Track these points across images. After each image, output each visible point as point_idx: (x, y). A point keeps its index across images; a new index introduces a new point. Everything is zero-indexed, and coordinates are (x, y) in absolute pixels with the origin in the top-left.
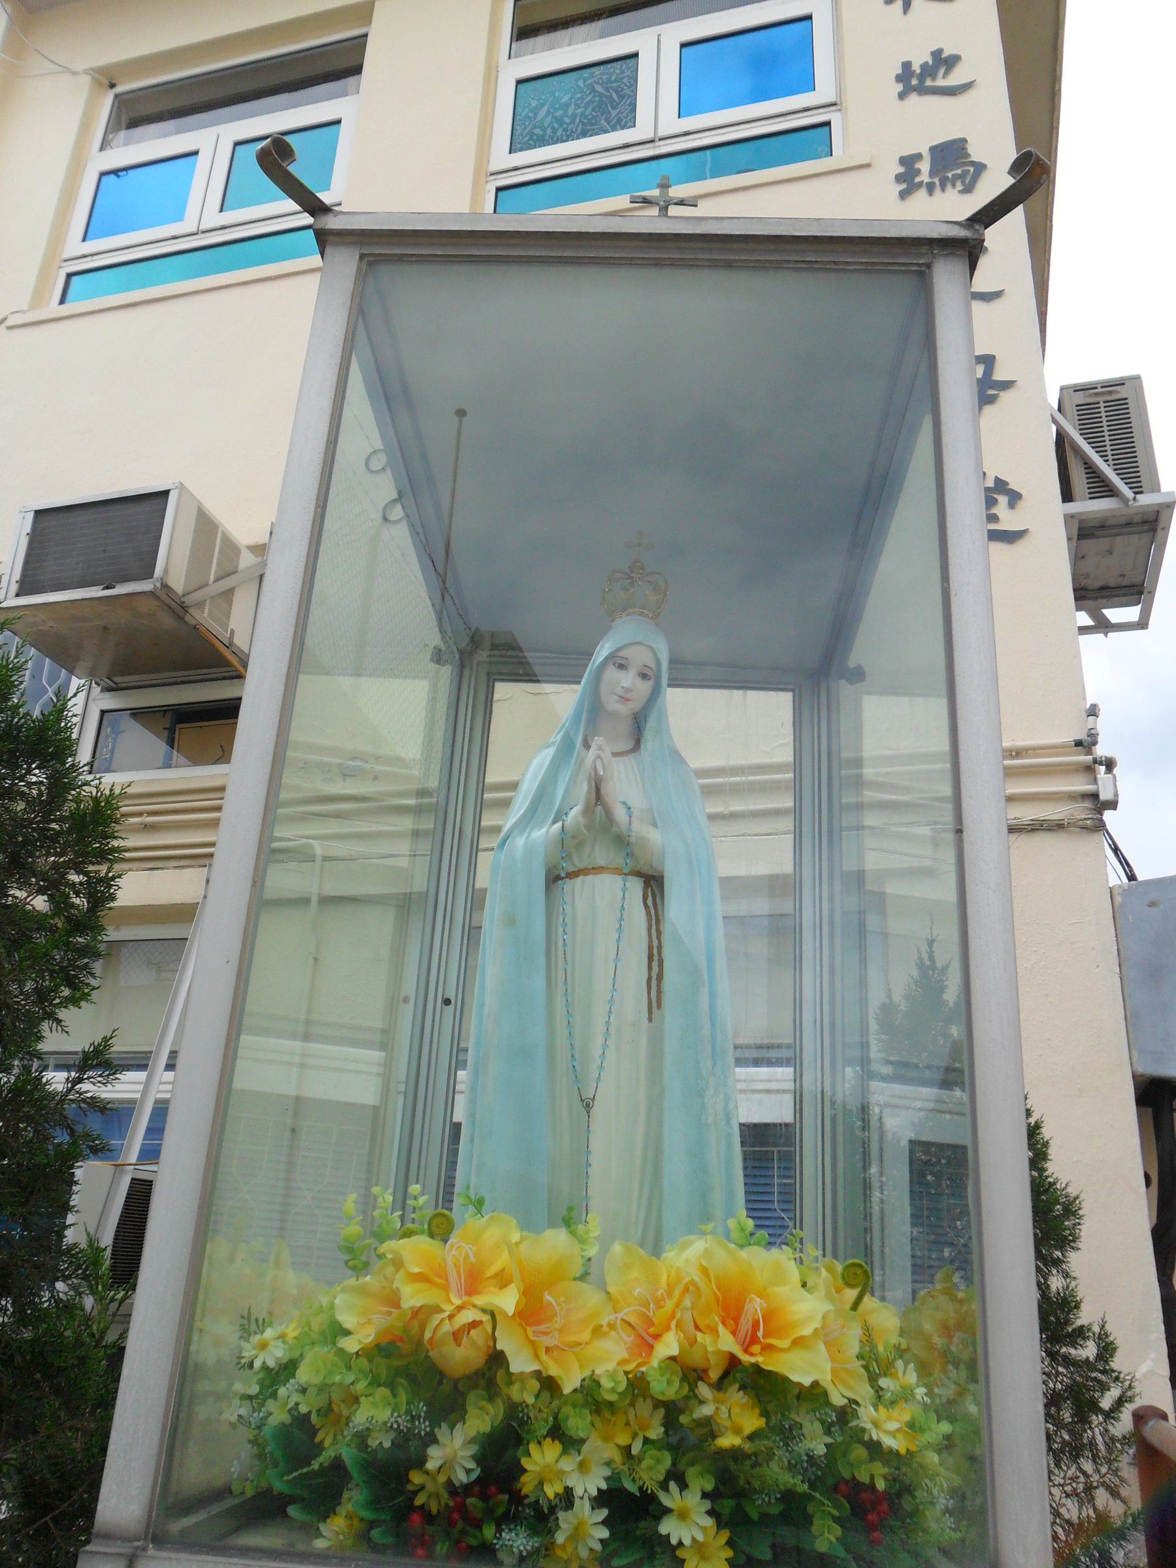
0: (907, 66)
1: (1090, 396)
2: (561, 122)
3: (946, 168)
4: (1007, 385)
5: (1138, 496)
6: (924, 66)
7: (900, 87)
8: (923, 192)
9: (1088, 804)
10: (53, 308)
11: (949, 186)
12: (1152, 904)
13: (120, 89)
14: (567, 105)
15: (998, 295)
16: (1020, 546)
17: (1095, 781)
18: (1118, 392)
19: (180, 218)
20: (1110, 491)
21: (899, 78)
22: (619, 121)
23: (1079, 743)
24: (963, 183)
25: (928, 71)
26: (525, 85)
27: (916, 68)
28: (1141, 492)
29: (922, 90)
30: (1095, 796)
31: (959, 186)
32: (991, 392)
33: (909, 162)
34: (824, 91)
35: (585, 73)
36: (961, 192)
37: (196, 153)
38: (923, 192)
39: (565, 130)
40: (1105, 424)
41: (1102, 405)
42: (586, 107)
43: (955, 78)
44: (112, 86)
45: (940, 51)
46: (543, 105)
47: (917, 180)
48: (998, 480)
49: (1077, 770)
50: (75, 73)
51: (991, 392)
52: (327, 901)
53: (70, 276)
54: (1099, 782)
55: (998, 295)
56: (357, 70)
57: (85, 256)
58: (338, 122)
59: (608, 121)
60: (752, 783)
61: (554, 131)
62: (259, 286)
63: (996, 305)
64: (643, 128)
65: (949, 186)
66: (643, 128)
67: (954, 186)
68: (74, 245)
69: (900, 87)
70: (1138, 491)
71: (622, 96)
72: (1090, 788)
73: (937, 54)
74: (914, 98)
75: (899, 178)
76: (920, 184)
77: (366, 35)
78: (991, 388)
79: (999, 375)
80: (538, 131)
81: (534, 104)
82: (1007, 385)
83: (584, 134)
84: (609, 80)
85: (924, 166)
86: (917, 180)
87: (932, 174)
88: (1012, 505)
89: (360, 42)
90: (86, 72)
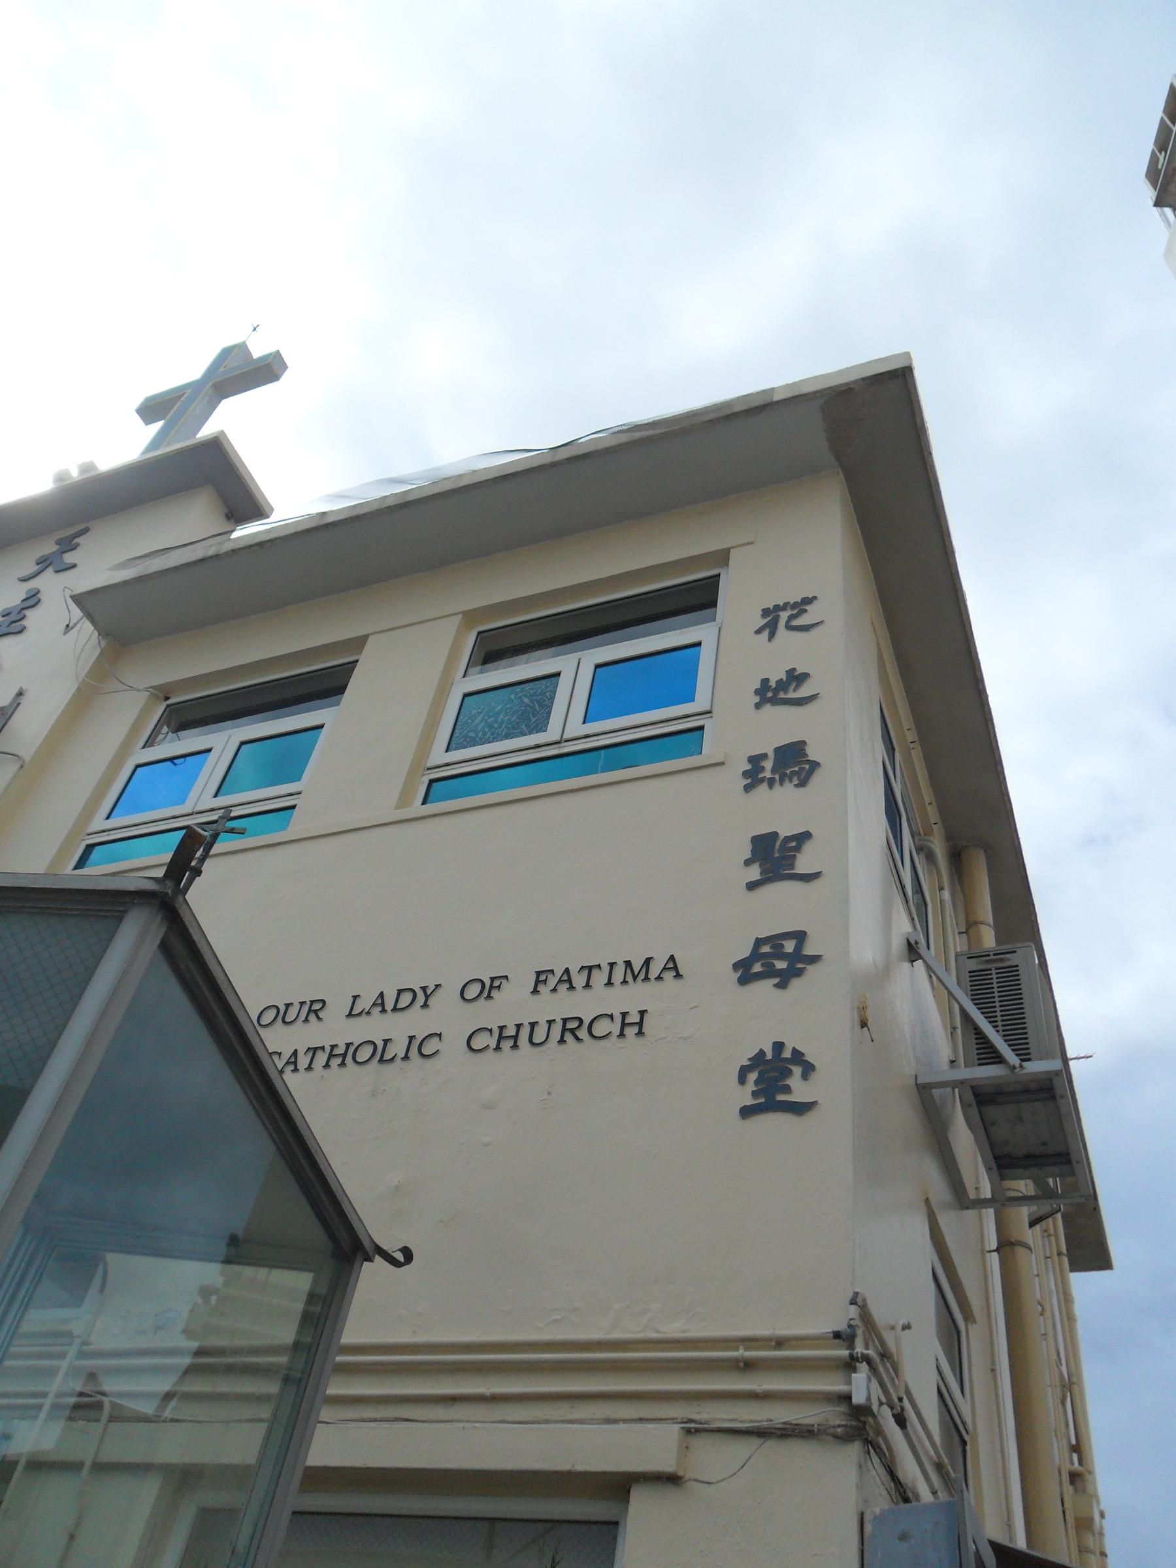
0: (765, 681)
1: (983, 962)
2: (490, 727)
3: (786, 766)
4: (814, 959)
5: (1025, 1064)
6: (780, 682)
7: (757, 699)
8: (765, 786)
9: (843, 1408)
10: (417, 809)
11: (787, 780)
12: (903, 1537)
13: (169, 702)
14: (499, 713)
15: (816, 876)
16: (810, 1118)
17: (849, 1383)
18: (1008, 960)
19: (692, 699)
20: (998, 1059)
21: (757, 692)
22: (536, 727)
23: (837, 1335)
24: (799, 778)
25: (782, 685)
26: (248, 746)
27: (773, 684)
28: (1029, 1060)
29: (776, 701)
30: (847, 1398)
31: (796, 781)
32: (800, 966)
33: (756, 761)
34: (701, 702)
35: (518, 688)
36: (796, 786)
37: (322, 726)
38: (765, 786)
39: (493, 734)
40: (995, 985)
41: (994, 972)
42: (513, 715)
43: (803, 692)
44: (167, 699)
45: (794, 670)
46: (479, 713)
47: (761, 776)
48: (795, 1051)
49: (838, 1367)
50: (139, 690)
51: (800, 966)
52: (100, 1468)
53: (432, 782)
54: (853, 1382)
55: (816, 876)
56: (713, 604)
57: (103, 831)
58: (558, 674)
59: (527, 726)
60: (382, 1364)
61: (484, 734)
62: (688, 774)
63: (814, 884)
64: (553, 732)
65: (787, 780)
66: (553, 732)
67: (791, 781)
68: (438, 755)
69: (757, 699)
70: (1025, 1057)
71: (542, 706)
72: (841, 1388)
73: (791, 672)
74: (768, 709)
75: (746, 774)
76: (762, 780)
77: (719, 575)
78: (800, 962)
79: (809, 950)
80: (472, 734)
81: (474, 712)
82: (814, 959)
83: (508, 736)
84: (535, 694)
85: (768, 765)
86: (761, 776)
87: (773, 771)
88: (805, 1076)
89: (714, 581)
90: (146, 689)
